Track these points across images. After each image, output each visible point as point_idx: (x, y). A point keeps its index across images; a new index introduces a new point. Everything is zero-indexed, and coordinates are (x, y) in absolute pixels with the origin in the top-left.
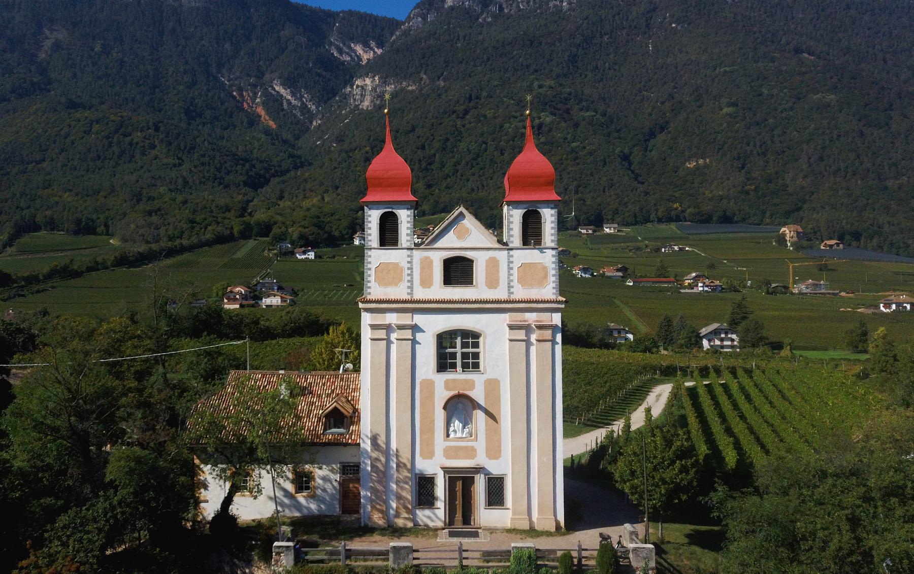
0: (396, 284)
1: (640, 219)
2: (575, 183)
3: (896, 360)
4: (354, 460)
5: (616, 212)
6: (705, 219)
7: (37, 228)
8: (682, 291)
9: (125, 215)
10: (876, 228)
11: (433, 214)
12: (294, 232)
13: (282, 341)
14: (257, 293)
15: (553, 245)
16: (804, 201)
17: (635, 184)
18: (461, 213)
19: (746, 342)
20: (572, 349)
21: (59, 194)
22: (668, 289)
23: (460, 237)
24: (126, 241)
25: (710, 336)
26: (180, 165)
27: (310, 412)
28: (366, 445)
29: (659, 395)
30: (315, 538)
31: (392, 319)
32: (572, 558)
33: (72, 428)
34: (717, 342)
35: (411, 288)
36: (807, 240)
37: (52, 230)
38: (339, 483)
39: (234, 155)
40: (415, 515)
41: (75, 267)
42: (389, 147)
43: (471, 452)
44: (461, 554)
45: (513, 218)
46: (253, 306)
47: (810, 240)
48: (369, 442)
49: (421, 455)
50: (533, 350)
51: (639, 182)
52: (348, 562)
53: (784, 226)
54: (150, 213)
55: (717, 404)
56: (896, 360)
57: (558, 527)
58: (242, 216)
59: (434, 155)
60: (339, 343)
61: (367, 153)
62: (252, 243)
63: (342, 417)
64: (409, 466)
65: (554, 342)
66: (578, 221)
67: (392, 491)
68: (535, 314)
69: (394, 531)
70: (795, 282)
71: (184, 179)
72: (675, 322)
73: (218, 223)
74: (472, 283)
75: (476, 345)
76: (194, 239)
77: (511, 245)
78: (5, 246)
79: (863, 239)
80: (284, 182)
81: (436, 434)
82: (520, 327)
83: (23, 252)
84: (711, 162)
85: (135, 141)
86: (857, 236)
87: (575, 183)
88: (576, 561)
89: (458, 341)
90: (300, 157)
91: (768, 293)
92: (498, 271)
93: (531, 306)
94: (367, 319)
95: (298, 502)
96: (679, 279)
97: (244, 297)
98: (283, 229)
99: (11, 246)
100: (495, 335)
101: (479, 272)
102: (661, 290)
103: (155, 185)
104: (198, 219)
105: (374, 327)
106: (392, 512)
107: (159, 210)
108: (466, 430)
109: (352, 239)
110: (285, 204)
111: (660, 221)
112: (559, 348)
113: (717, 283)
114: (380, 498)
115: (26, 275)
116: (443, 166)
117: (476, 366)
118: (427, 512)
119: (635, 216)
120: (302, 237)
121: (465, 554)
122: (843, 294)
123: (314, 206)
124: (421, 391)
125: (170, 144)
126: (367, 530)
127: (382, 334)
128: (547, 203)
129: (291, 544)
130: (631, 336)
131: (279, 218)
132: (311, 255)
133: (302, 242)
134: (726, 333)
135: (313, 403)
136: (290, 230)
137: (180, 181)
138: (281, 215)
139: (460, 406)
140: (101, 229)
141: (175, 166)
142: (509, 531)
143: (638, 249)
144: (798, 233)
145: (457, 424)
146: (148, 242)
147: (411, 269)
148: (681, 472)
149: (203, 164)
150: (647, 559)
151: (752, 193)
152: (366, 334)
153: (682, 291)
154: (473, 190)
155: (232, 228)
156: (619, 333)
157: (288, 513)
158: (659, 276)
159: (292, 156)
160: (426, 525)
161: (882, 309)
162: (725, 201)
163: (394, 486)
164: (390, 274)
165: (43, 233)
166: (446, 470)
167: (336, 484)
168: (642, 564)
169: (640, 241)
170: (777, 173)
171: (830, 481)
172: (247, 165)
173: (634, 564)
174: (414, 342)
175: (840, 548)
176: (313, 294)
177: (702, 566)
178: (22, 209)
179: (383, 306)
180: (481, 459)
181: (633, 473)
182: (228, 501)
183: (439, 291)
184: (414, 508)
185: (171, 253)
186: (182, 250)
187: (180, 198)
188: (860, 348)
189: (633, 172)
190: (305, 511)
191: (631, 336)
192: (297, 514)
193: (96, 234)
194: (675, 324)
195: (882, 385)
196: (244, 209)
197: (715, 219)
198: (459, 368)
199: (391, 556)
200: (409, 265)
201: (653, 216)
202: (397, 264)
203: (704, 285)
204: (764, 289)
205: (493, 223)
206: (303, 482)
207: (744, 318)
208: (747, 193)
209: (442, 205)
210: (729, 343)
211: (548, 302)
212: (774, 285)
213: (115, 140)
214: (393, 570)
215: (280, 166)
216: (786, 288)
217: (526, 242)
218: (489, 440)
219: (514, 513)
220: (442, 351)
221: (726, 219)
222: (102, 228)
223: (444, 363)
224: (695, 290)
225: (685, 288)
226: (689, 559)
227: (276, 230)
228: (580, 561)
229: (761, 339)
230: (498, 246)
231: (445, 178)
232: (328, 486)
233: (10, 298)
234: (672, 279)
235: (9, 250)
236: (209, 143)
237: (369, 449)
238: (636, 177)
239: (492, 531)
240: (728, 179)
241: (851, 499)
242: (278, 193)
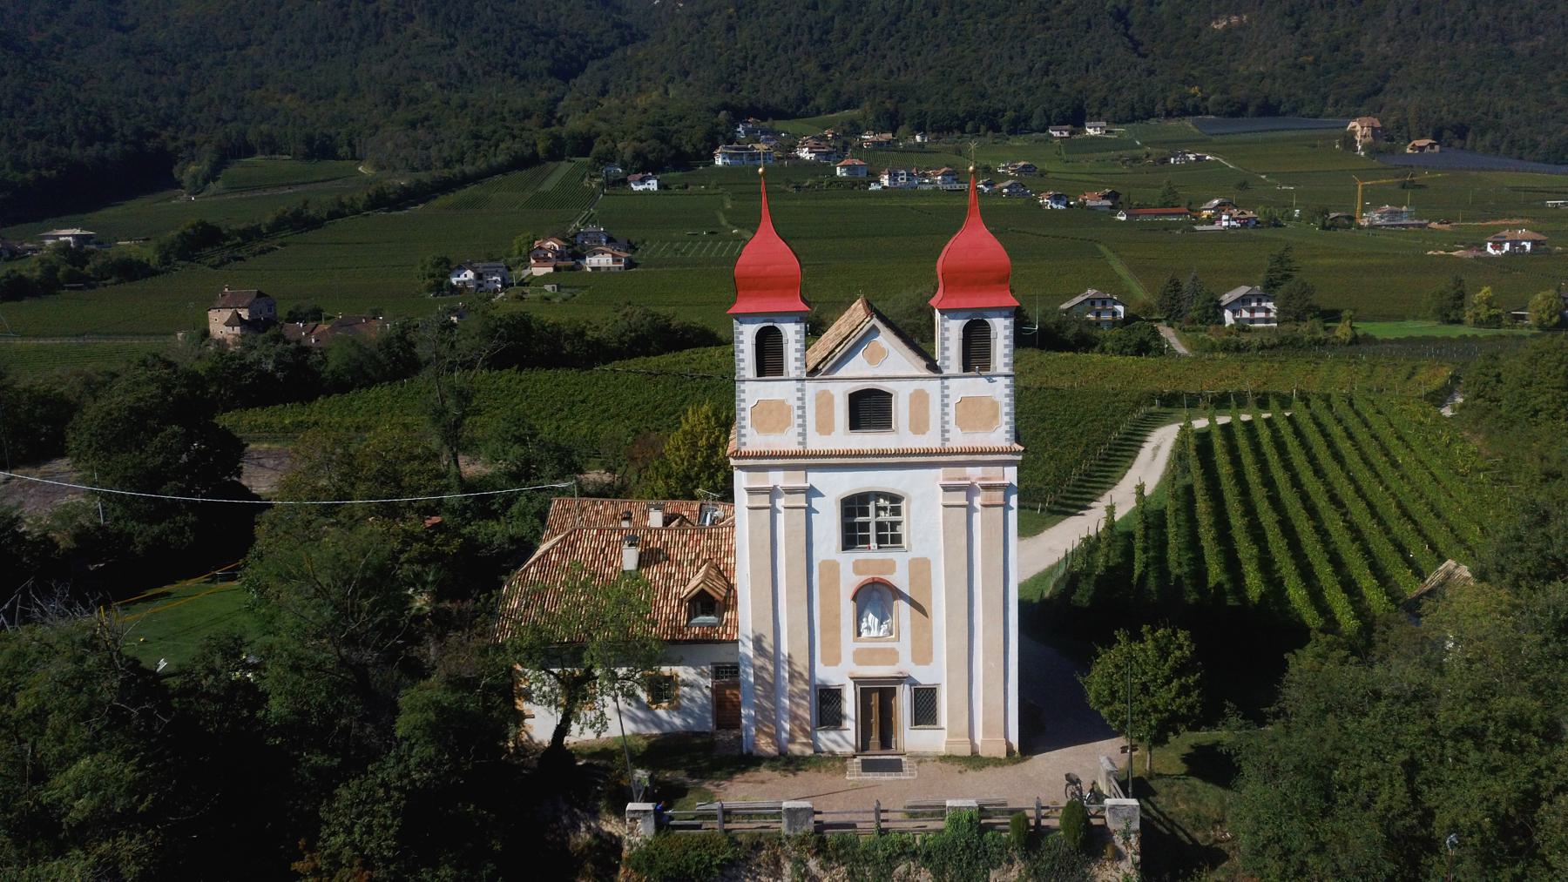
0: (782, 430)
1: (1139, 113)
2: (1045, 58)
3: (1499, 381)
4: (731, 659)
5: (1104, 103)
6: (1237, 111)
7: (250, 152)
8: (1198, 228)
9: (377, 127)
10: (1491, 118)
11: (832, 112)
12: (626, 148)
13: (618, 365)
14: (577, 248)
15: (1007, 371)
16: (1386, 79)
17: (1134, 58)
18: (874, 328)
19: (1289, 313)
20: (1034, 355)
21: (278, 96)
22: (1177, 225)
23: (873, 360)
24: (384, 168)
25: (1235, 306)
26: (453, 46)
27: (667, 589)
28: (747, 649)
29: (1157, 448)
30: (681, 775)
31: (777, 479)
32: (1027, 819)
33: (343, 662)
34: (1246, 314)
35: (803, 434)
36: (1387, 140)
37: (273, 153)
38: (712, 690)
39: (532, 27)
40: (815, 739)
41: (312, 212)
42: (766, 226)
43: (891, 656)
44: (878, 816)
45: (949, 334)
46: (572, 269)
47: (1392, 140)
48: (750, 645)
49: (823, 660)
50: (977, 517)
51: (1140, 55)
52: (727, 826)
53: (1354, 117)
54: (413, 125)
55: (1236, 460)
56: (1499, 381)
57: (1010, 752)
58: (548, 124)
59: (832, 18)
60: (702, 432)
61: (730, 17)
62: (565, 167)
63: (712, 602)
64: (806, 675)
65: (1006, 507)
66: (1048, 118)
67: (784, 708)
68: (979, 469)
69: (788, 763)
70: (1365, 209)
71: (460, 68)
72: (1186, 284)
73: (514, 137)
74: (890, 426)
75: (896, 511)
76: (482, 164)
77: (946, 372)
78: (206, 181)
79: (1470, 136)
80: (607, 67)
81: (843, 631)
82: (958, 488)
83: (232, 188)
84: (1249, 21)
85: (383, 9)
86: (1461, 132)
87: (1045, 58)
88: (1032, 823)
89: (872, 506)
90: (629, 27)
91: (1324, 227)
92: (927, 409)
93: (974, 457)
94: (741, 480)
95: (657, 716)
96: (1193, 209)
97: (559, 255)
98: (610, 144)
99: (215, 180)
100: (924, 500)
101: (901, 410)
102: (1168, 227)
103: (418, 80)
104: (486, 131)
105: (751, 491)
106: (784, 735)
107: (427, 118)
108: (884, 627)
109: (712, 157)
110: (609, 102)
111: (1169, 114)
112: (1013, 516)
113: (1250, 214)
114: (768, 718)
115: (242, 226)
116: (845, 35)
117: (897, 539)
118: (833, 735)
119: (1133, 109)
120: (638, 155)
121: (883, 816)
122: (1434, 225)
123: (653, 104)
124: (821, 576)
125: (434, 13)
126: (748, 761)
127: (764, 500)
128: (999, 311)
129: (649, 806)
130: (1120, 308)
131: (602, 126)
132: (653, 185)
133: (638, 165)
134: (1259, 301)
135: (671, 575)
136: (620, 146)
137: (454, 71)
138: (605, 121)
139: (875, 596)
140: (343, 150)
141: (444, 48)
142: (947, 759)
143: (1136, 159)
144: (1374, 129)
145: (871, 619)
146: (414, 170)
147: (802, 408)
148: (1178, 695)
149: (487, 43)
150: (1128, 820)
151: (1308, 68)
152: (741, 498)
153: (1198, 228)
154: (891, 72)
155: (535, 144)
156: (1104, 303)
157: (644, 730)
158: (1165, 205)
159: (617, 25)
160: (832, 752)
161: (1490, 250)
162: (1268, 81)
163: (787, 702)
164: (773, 416)
165: (258, 159)
166: (857, 681)
167: (707, 692)
168: (1122, 826)
169: (1138, 147)
170: (1348, 35)
171: (1382, 707)
172: (552, 42)
173: (1111, 826)
174: (809, 511)
175: (1390, 808)
176: (659, 248)
177: (1203, 811)
178: (225, 122)
179: (764, 461)
180: (904, 664)
181: (1113, 694)
182: (562, 731)
183: (844, 439)
184: (814, 729)
185: (446, 186)
186: (465, 181)
187: (456, 99)
188: (1452, 316)
189: (1131, 38)
190: (667, 728)
191: (1120, 308)
192: (656, 731)
193: (337, 158)
194: (1184, 288)
195: (1476, 423)
196: (551, 113)
197: (1251, 109)
198: (873, 544)
199: (785, 820)
200: (799, 403)
201: (1158, 108)
202: (783, 402)
203: (1231, 218)
204: (1319, 221)
205: (918, 338)
206: (662, 689)
207: (1287, 277)
208: (1302, 68)
209: (844, 98)
210: (1262, 315)
211: (998, 453)
212: (1333, 215)
213: (352, 9)
214: (788, 837)
215: (600, 42)
216: (1351, 218)
217: (967, 366)
218: (915, 639)
219: (949, 735)
220: (849, 520)
221: (1268, 110)
222: (346, 148)
223: (852, 537)
224: (1216, 227)
225: (1203, 222)
226: (1186, 801)
227: (598, 147)
228: (1038, 822)
229: (1311, 308)
230: (927, 373)
231: (850, 55)
232: (697, 694)
233: (222, 263)
234: (1185, 210)
235: (213, 187)
236: (494, 10)
237: (751, 654)
238: (1136, 45)
239: (920, 759)
240: (1275, 46)
241: (1411, 734)
242: (599, 85)
